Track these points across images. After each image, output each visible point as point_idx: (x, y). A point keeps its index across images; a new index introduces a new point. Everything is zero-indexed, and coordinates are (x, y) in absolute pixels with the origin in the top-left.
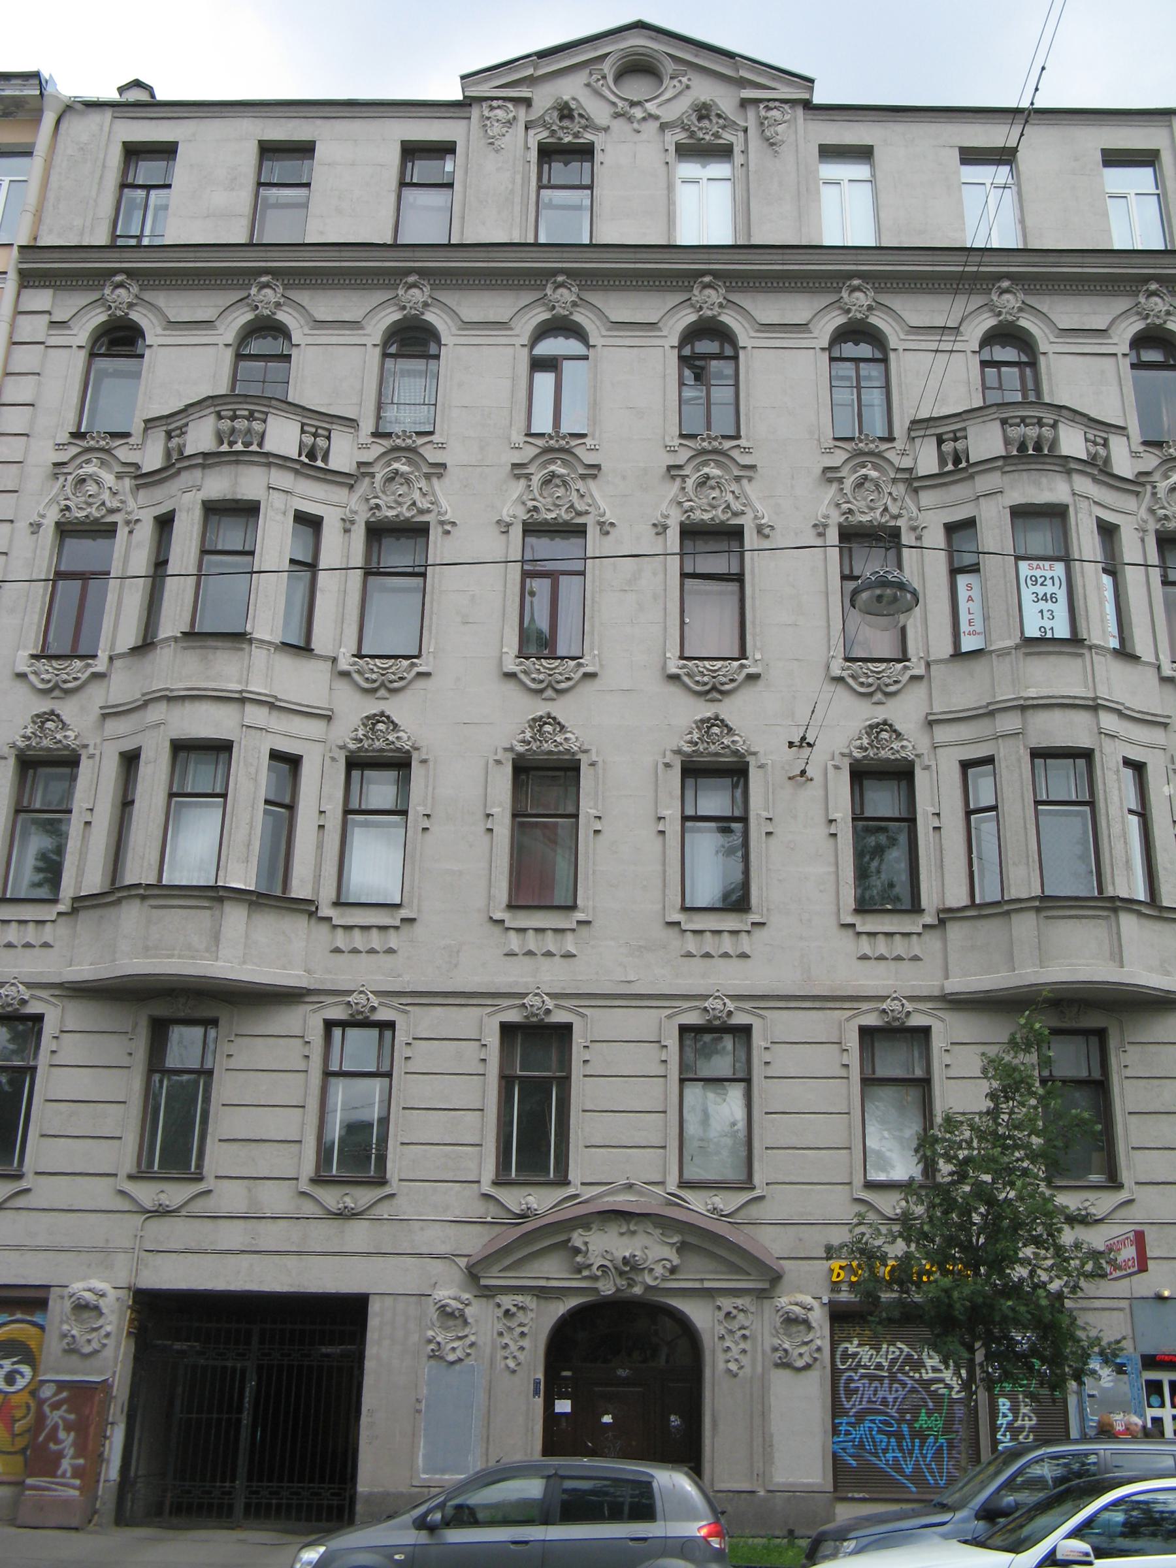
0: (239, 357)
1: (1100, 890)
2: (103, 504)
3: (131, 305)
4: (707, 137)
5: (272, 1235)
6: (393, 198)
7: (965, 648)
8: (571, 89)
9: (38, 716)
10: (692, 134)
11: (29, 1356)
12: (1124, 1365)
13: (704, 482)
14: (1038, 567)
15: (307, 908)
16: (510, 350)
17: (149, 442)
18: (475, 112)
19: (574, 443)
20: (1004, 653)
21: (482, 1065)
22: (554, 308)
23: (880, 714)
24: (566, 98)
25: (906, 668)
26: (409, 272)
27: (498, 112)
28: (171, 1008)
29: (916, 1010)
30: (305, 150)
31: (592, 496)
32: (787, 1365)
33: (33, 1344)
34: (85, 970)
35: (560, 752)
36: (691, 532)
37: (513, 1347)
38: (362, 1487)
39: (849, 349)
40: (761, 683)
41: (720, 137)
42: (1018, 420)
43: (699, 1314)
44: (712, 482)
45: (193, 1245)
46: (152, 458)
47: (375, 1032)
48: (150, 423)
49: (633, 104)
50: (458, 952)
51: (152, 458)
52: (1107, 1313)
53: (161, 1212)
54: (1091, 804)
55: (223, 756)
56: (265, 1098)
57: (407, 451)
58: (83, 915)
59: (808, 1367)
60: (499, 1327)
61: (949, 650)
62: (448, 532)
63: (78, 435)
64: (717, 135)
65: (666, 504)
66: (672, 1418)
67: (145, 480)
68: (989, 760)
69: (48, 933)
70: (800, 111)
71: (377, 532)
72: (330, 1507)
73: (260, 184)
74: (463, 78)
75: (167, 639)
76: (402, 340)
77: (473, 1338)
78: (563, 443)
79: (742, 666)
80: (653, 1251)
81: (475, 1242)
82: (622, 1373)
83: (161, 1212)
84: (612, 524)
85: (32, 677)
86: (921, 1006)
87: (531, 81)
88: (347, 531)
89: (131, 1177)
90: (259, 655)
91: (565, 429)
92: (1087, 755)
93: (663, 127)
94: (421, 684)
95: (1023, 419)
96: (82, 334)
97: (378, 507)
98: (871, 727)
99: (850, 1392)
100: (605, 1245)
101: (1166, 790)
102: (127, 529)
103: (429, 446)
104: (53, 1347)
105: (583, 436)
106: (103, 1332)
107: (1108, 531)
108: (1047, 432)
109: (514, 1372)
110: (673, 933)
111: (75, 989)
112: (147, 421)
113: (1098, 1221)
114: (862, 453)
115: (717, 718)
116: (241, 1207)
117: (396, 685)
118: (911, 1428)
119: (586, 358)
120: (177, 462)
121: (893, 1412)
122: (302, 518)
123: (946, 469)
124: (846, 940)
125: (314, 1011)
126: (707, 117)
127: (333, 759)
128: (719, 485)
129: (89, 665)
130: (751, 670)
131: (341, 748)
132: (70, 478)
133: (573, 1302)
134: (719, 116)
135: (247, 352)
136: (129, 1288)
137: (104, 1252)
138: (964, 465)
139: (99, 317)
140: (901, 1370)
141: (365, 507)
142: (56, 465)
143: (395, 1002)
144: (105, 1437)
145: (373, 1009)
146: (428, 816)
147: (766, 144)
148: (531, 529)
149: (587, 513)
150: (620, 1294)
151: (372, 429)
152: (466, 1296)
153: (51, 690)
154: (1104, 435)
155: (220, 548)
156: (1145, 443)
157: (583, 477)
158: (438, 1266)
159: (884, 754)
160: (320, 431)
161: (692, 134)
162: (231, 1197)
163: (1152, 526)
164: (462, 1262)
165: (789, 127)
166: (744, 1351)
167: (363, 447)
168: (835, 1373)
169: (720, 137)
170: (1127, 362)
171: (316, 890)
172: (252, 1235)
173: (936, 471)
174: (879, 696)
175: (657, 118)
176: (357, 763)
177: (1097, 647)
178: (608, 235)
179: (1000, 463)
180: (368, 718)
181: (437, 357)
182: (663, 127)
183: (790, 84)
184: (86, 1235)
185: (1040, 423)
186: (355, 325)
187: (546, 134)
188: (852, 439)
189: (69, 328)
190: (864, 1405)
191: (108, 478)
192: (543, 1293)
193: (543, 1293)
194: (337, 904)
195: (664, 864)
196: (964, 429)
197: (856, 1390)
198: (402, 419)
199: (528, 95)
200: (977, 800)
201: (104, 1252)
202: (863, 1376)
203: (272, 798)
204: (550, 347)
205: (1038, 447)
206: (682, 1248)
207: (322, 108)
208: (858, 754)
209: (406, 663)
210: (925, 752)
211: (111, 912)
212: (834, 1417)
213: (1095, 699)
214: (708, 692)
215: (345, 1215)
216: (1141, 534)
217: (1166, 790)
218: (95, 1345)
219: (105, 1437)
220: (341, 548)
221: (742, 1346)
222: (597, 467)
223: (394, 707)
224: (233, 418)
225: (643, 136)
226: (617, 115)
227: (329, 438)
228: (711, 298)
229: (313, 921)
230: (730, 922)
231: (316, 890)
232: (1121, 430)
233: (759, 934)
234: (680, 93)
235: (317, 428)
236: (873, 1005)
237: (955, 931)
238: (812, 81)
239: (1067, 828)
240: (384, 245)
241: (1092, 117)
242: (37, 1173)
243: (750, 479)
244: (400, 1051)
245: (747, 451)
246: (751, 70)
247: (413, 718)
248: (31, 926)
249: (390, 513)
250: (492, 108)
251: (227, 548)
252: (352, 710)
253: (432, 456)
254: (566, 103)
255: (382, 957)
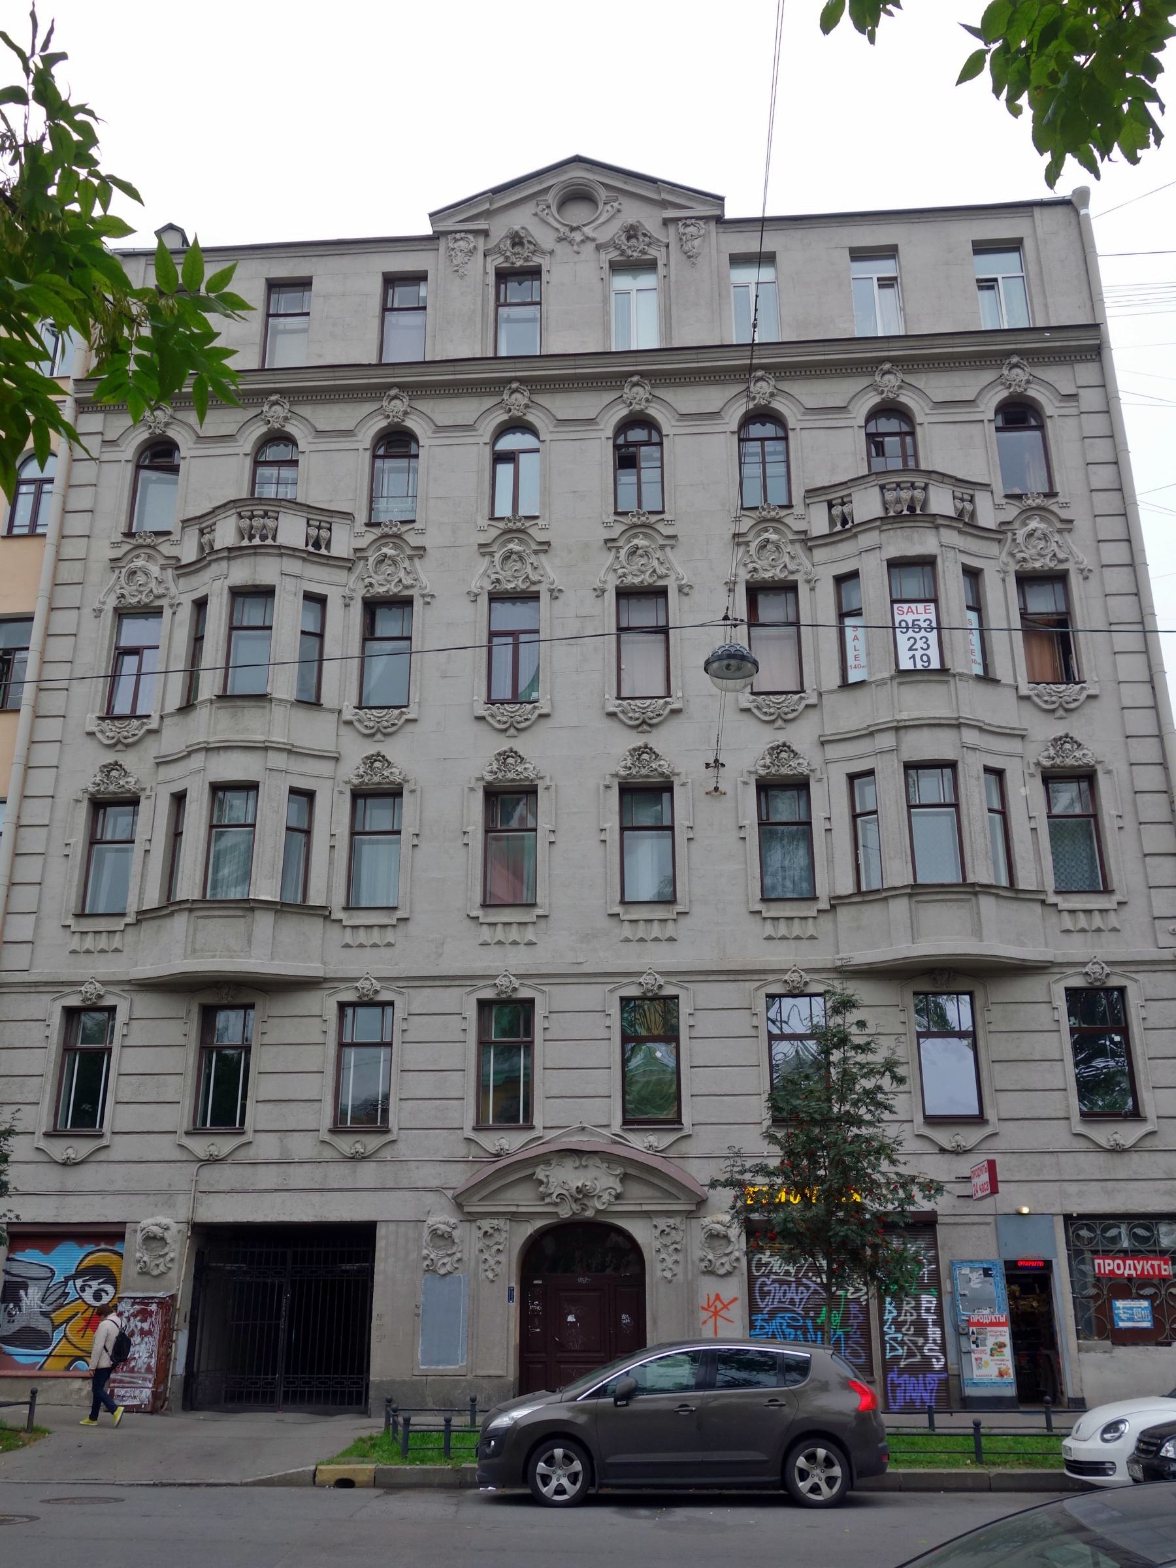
0: (257, 463)
1: (964, 878)
2: (151, 591)
3: (167, 424)
4: (635, 254)
5: (300, 1176)
6: (376, 322)
7: (851, 681)
8: (521, 219)
9: (105, 766)
10: (623, 253)
11: (112, 1279)
12: (990, 1269)
13: (634, 551)
14: (910, 611)
15: (323, 913)
16: (475, 448)
17: (186, 538)
18: (442, 244)
19: (528, 524)
20: (881, 683)
21: (462, 1033)
22: (510, 410)
23: (781, 737)
24: (517, 228)
25: (802, 698)
26: (391, 386)
27: (461, 243)
28: (215, 996)
29: (812, 980)
30: (305, 284)
31: (543, 568)
32: (712, 1273)
33: (114, 1269)
34: (148, 969)
35: (521, 780)
36: (625, 594)
37: (492, 1262)
38: (373, 1377)
39: (756, 430)
40: (681, 716)
41: (646, 253)
42: (894, 485)
43: (640, 1232)
44: (640, 552)
45: (238, 1187)
46: (189, 553)
47: (378, 1010)
48: (186, 522)
49: (573, 229)
50: (443, 944)
51: (189, 553)
52: (976, 1227)
53: (213, 1161)
54: (956, 806)
55: (252, 794)
56: (291, 1066)
57: (392, 536)
58: (145, 925)
59: (729, 1274)
60: (480, 1245)
61: (838, 681)
62: (428, 603)
63: (129, 534)
64: (643, 252)
65: (605, 572)
66: (624, 1317)
67: (184, 570)
68: (870, 773)
69: (117, 941)
70: (713, 225)
71: (372, 606)
72: (351, 1393)
73: (269, 315)
74: (431, 215)
75: (204, 702)
76: (388, 443)
77: (458, 1255)
78: (519, 524)
79: (667, 703)
80: (601, 1182)
81: (459, 1177)
82: (581, 1280)
83: (213, 1161)
84: (560, 590)
85: (99, 735)
86: (816, 976)
87: (488, 214)
88: (347, 605)
89: (187, 1133)
90: (278, 712)
91: (522, 512)
92: (952, 765)
93: (598, 248)
94: (410, 728)
95: (898, 484)
96: (129, 450)
97: (371, 585)
98: (773, 748)
99: (764, 1294)
100: (565, 1178)
101: (1023, 791)
102: (171, 611)
103: (412, 532)
104: (128, 1272)
105: (536, 517)
106: (168, 1258)
107: (973, 575)
108: (918, 494)
109: (492, 1281)
110: (613, 923)
111: (139, 985)
112: (184, 522)
113: (966, 1152)
114: (766, 520)
115: (646, 747)
116: (275, 1155)
117: (389, 730)
118: (815, 1323)
119: (537, 451)
120: (208, 556)
121: (799, 1311)
122: (309, 597)
123: (836, 530)
124: (754, 925)
125: (329, 995)
126: (635, 236)
127: (341, 792)
128: (646, 554)
129: (144, 724)
130: (675, 706)
131: (346, 783)
132: (124, 571)
133: (539, 1224)
134: (645, 235)
135: (263, 459)
136: (188, 1223)
137: (167, 1195)
138: (850, 524)
139: (142, 435)
140: (805, 1276)
141: (361, 585)
142: (112, 560)
143: (394, 985)
144: (172, 1341)
145: (376, 992)
146: (417, 835)
147: (684, 257)
148: (495, 597)
149: (540, 582)
150: (576, 1217)
151: (365, 520)
152: (452, 1221)
153: (115, 745)
154: (971, 492)
155: (245, 624)
156: (1007, 496)
157: (536, 552)
158: (430, 1198)
159: (784, 771)
160: (323, 524)
161: (623, 253)
162: (266, 1147)
163: (1013, 567)
164: (450, 1193)
165: (704, 241)
166: (676, 1262)
167: (359, 535)
168: (751, 1279)
169: (646, 253)
170: (993, 426)
171: (328, 898)
172: (282, 1180)
173: (827, 531)
174: (779, 723)
175: (593, 240)
176: (359, 795)
177: (960, 675)
178: (558, 345)
179: (878, 523)
180: (367, 758)
181: (416, 456)
182: (598, 248)
183: (704, 203)
184: (154, 1183)
185: (913, 486)
186: (349, 433)
187: (501, 259)
188: (757, 508)
189: (118, 445)
190: (776, 1305)
191: (155, 570)
192: (515, 1217)
193: (515, 1217)
194: (347, 908)
195: (606, 867)
196: (850, 495)
197: (769, 1292)
198: (390, 510)
199: (486, 227)
200: (863, 803)
201: (167, 1195)
202: (774, 1281)
203: (294, 824)
204: (508, 443)
205: (911, 508)
206: (624, 1178)
207: (315, 248)
208: (762, 772)
209: (396, 712)
210: (818, 767)
211: (168, 922)
212: (750, 1315)
213: (957, 719)
214: (640, 725)
215: (357, 1158)
216: (1002, 575)
217: (1023, 791)
218: (162, 1268)
219: (172, 1341)
220: (343, 625)
221: (675, 1257)
222: (548, 543)
223: (388, 749)
224: (251, 518)
225: (583, 256)
226: (560, 240)
227: (330, 529)
228: (637, 396)
229: (328, 923)
230: (659, 913)
231: (328, 898)
232: (985, 486)
233: (683, 921)
234: (613, 217)
235: (320, 521)
236: (776, 977)
237: (843, 913)
238: (722, 199)
239: (935, 828)
240: (370, 365)
241: (964, 213)
242: (113, 1133)
243: (673, 547)
244: (399, 1025)
245: (670, 523)
246: (672, 192)
247: (404, 757)
248: (104, 935)
249: (382, 590)
250: (456, 240)
251: (252, 624)
252: (355, 751)
253: (413, 540)
254: (517, 232)
255: (383, 950)
